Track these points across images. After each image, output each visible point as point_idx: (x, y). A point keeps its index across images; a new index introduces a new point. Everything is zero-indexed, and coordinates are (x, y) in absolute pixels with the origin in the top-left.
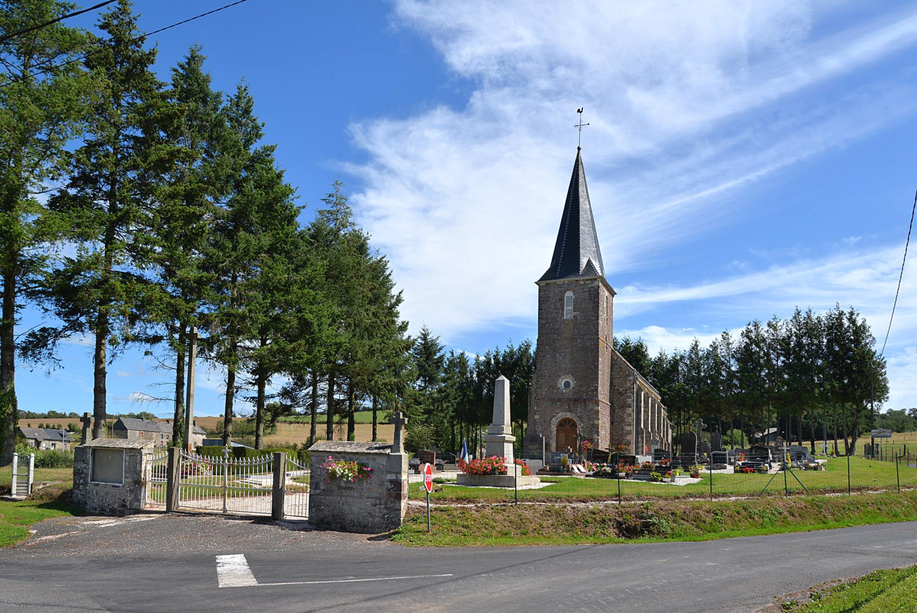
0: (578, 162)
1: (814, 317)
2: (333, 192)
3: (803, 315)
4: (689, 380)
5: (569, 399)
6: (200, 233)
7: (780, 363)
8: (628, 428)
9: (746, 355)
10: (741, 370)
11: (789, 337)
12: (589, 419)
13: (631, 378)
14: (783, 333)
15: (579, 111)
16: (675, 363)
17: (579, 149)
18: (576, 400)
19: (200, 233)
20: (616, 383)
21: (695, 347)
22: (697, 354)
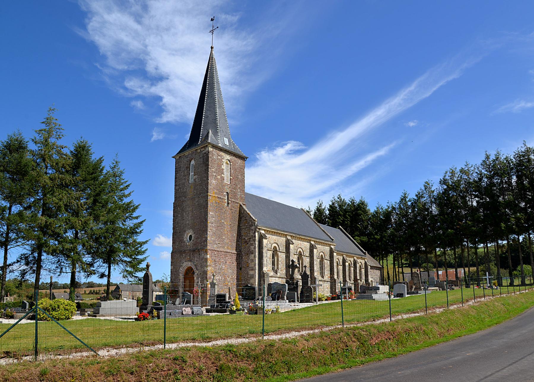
0: (211, 58)
1: (502, 158)
2: (48, 116)
3: (492, 157)
4: (399, 224)
5: (190, 250)
6: (458, 190)
7: (475, 204)
8: (251, 273)
9: (443, 200)
10: (442, 212)
11: (480, 179)
12: (202, 267)
13: (253, 228)
14: (475, 177)
15: (212, 20)
16: (388, 215)
17: (212, 48)
18: (194, 251)
19: (458, 190)
20: (243, 232)
21: (403, 199)
22: (406, 204)
